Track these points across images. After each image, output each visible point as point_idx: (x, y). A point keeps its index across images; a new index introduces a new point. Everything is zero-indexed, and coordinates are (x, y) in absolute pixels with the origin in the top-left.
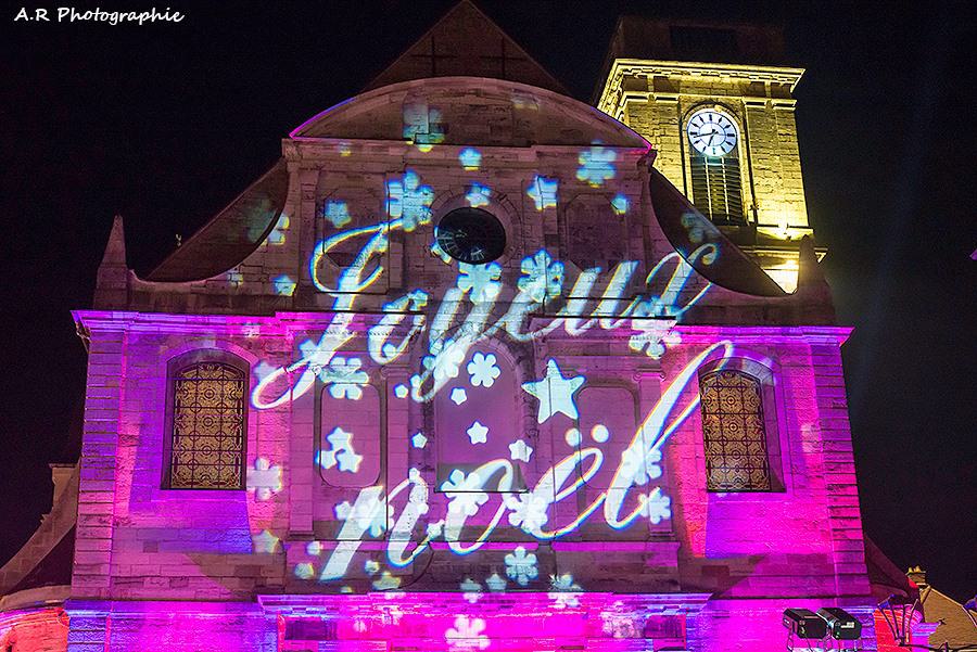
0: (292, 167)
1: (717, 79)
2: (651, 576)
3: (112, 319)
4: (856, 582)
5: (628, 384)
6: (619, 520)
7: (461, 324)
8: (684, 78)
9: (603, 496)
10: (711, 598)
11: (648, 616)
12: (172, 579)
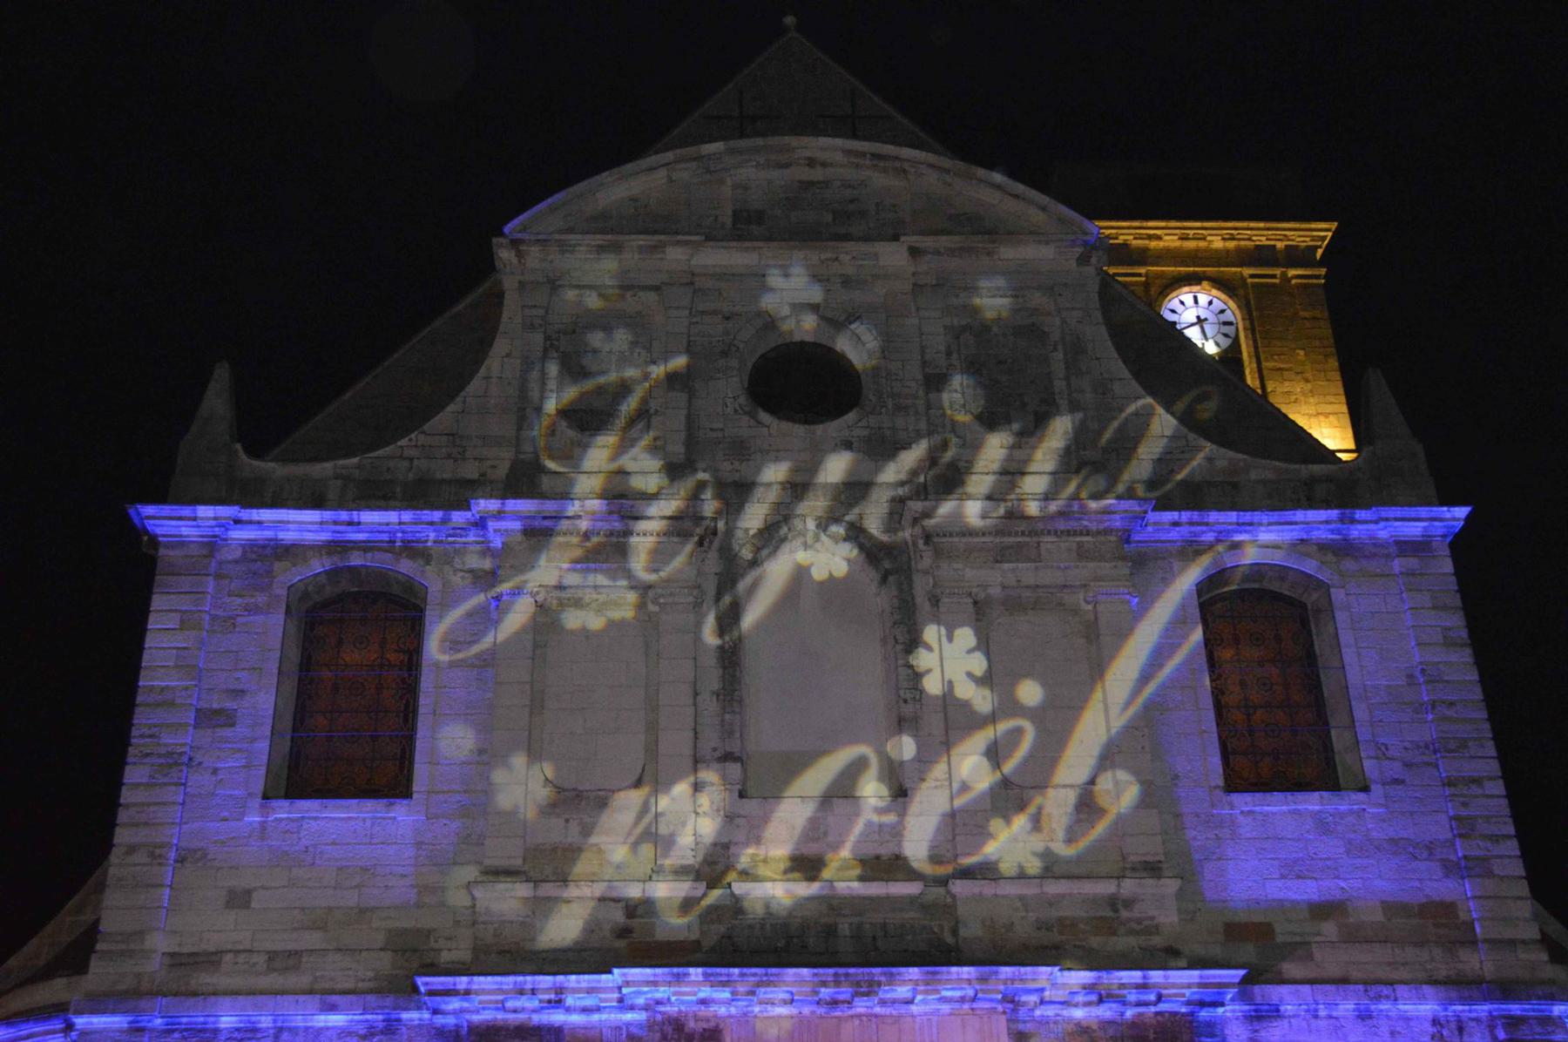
0: (509, 283)
1: (1202, 244)
2: (1132, 941)
3: (195, 519)
4: (1522, 956)
5: (1076, 612)
6: (1069, 840)
7: (786, 519)
8: (1153, 244)
9: (1038, 800)
10: (1245, 981)
11: (1129, 1013)
12: (272, 956)
